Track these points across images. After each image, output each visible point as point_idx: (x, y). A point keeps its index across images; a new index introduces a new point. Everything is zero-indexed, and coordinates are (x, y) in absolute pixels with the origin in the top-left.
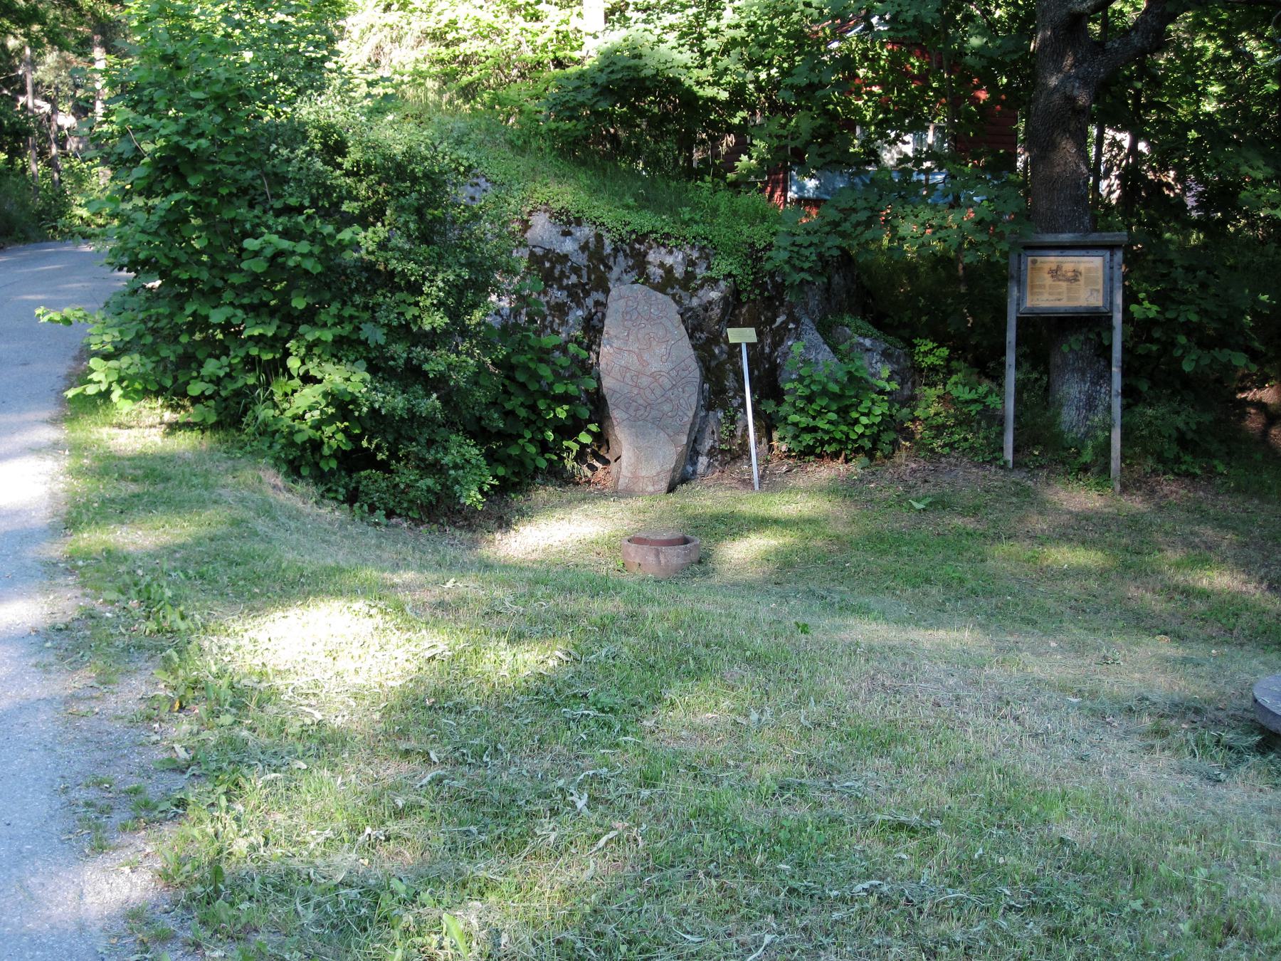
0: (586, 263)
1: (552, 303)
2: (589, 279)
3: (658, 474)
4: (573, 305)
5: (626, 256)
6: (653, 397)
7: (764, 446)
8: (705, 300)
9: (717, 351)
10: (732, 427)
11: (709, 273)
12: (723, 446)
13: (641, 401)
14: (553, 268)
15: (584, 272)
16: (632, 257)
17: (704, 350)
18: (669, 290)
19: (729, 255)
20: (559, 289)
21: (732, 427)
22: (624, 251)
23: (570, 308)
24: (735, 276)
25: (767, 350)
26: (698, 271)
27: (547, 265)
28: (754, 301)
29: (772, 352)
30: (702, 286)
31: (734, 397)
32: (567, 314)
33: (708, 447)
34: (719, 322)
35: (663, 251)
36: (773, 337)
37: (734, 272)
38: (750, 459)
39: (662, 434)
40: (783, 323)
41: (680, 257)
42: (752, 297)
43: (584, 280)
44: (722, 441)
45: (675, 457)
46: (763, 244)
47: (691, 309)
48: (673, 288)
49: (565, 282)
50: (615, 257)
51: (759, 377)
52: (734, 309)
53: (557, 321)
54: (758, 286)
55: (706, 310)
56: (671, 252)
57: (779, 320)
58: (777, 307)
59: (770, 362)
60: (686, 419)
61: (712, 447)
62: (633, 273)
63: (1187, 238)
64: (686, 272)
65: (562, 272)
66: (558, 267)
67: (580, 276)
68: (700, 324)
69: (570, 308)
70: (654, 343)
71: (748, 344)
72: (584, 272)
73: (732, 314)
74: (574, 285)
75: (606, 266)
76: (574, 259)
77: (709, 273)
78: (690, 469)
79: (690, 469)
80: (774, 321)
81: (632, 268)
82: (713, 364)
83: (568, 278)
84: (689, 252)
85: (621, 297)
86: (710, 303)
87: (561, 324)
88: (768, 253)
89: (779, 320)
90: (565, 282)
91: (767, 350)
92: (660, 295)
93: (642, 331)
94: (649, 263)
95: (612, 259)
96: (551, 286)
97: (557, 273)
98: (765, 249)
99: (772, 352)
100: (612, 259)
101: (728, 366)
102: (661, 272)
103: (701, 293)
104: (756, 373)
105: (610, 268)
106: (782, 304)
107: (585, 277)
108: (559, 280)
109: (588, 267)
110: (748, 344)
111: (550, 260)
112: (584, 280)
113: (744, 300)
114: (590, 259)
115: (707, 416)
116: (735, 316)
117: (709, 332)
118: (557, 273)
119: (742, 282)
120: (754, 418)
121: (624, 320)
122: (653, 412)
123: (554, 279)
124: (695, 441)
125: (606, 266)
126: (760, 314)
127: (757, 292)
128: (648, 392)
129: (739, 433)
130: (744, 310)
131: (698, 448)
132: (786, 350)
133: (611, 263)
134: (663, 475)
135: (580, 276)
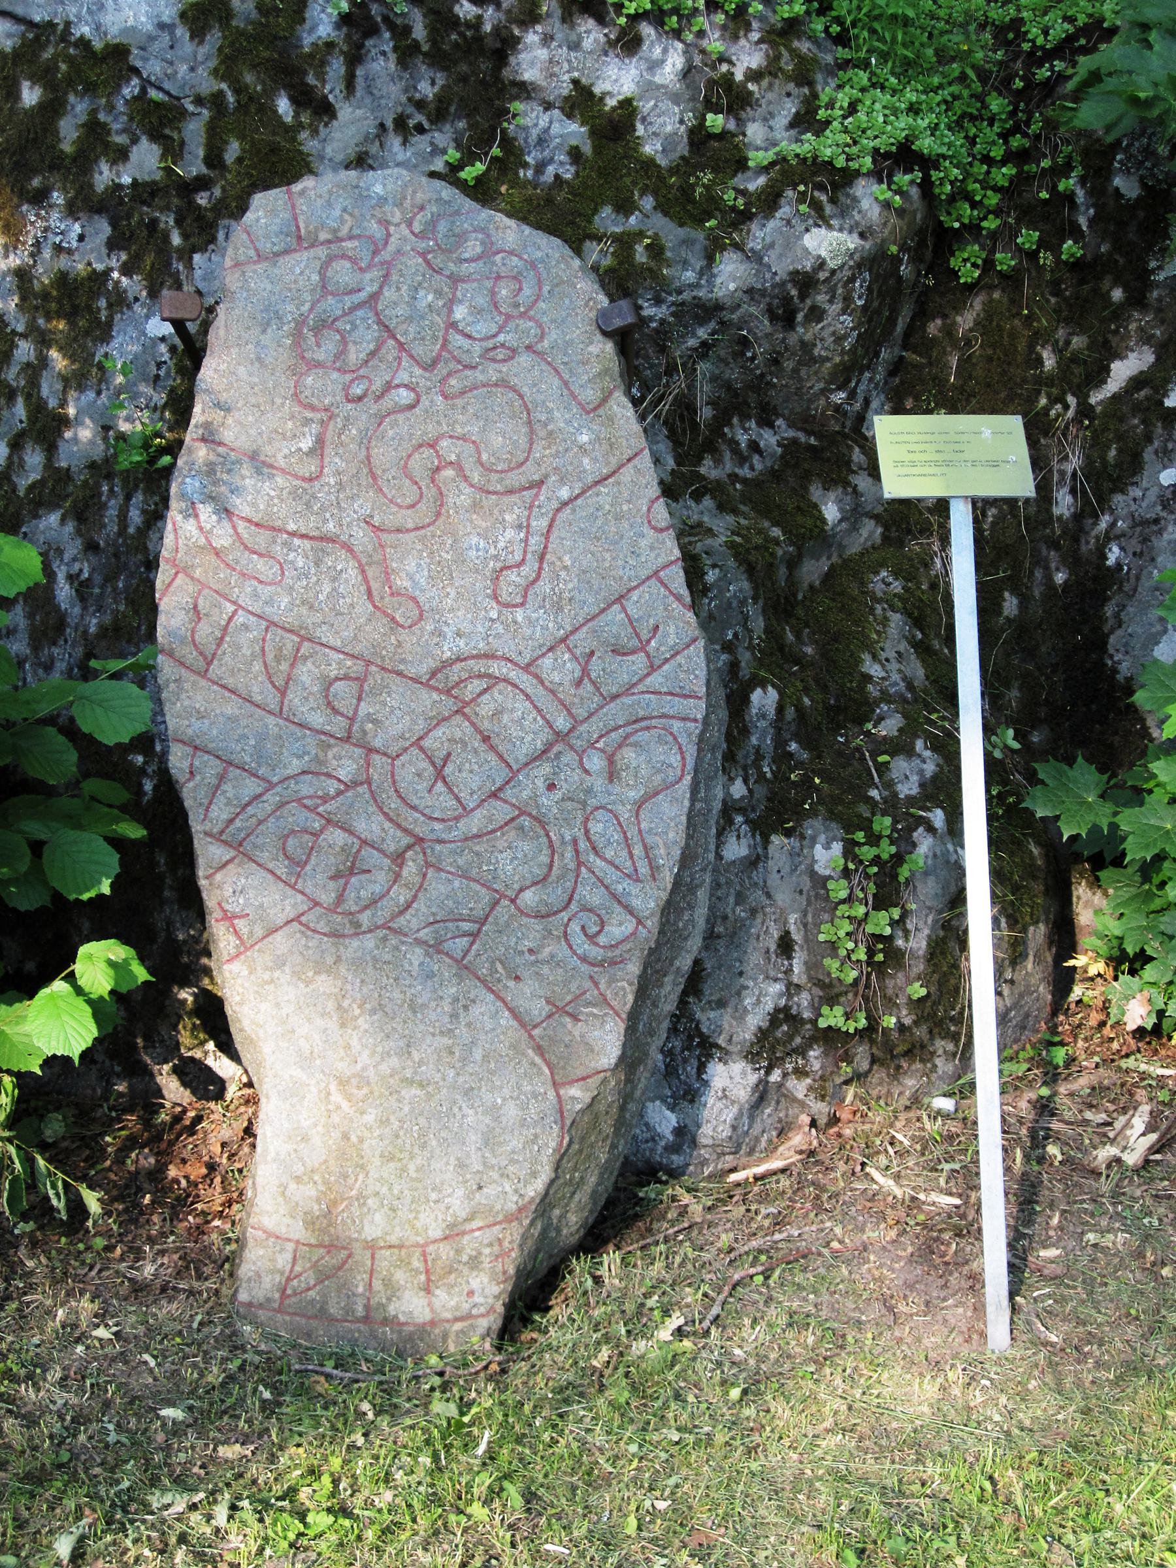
0: (207, 84)
1: (43, 276)
2: (214, 159)
3: (453, 1233)
4: (132, 285)
5: (406, 53)
6: (442, 802)
7: (1033, 971)
8: (781, 266)
9: (831, 512)
10: (881, 923)
11: (808, 144)
12: (833, 1017)
13: (370, 825)
14: (52, 108)
15: (194, 131)
16: (438, 58)
17: (765, 509)
18: (607, 219)
19: (908, 69)
20: (71, 211)
21: (881, 923)
22: (401, 32)
23: (120, 301)
24: (927, 163)
25: (1064, 504)
26: (755, 131)
27: (30, 96)
28: (1011, 280)
29: (1086, 513)
30: (769, 201)
31: (900, 746)
32: (104, 332)
33: (755, 1020)
34: (844, 376)
35: (591, 33)
36: (1096, 445)
37: (925, 144)
38: (965, 1055)
39: (484, 1008)
40: (1137, 382)
41: (675, 61)
42: (1005, 260)
43: (193, 166)
44: (830, 993)
45: (551, 1141)
46: (1060, 30)
47: (708, 311)
48: (625, 207)
49: (104, 175)
50: (355, 58)
51: (1022, 628)
52: (922, 314)
53: (58, 360)
54: (1030, 214)
55: (784, 315)
56: (629, 43)
57: (1122, 371)
58: (1118, 314)
59: (1073, 561)
60: (619, 928)
61: (782, 1015)
62: (442, 138)
63: (1058, 351)
64: (699, 137)
65: (94, 130)
66: (79, 107)
67: (173, 150)
68: (759, 385)
69: (120, 301)
70: (460, 497)
71: (980, 506)
72: (194, 131)
73: (913, 337)
74: (144, 192)
75: (305, 99)
76: (153, 68)
77: (808, 144)
78: (665, 1120)
79: (665, 1120)
80: (1100, 374)
81: (439, 113)
82: (813, 570)
83: (121, 155)
84: (715, 44)
85: (300, 240)
86: (805, 281)
87: (75, 381)
88: (1085, 63)
89: (1122, 371)
90: (104, 175)
91: (1064, 504)
92: (548, 247)
93: (400, 429)
94: (524, 90)
95: (337, 67)
96: (39, 198)
97: (69, 131)
98: (1067, 48)
99: (1086, 513)
100: (337, 67)
101: (886, 582)
102: (574, 131)
103: (760, 234)
104: (1010, 605)
105: (325, 111)
106: (1137, 300)
107: (197, 150)
108: (83, 161)
109: (217, 100)
110: (980, 506)
111: (44, 76)
112: (193, 166)
113: (969, 274)
114: (227, 68)
115: (754, 862)
116: (927, 346)
117: (803, 421)
118: (69, 131)
119: (961, 194)
120: (994, 843)
121: (304, 363)
122: (437, 886)
123: (57, 163)
124: (694, 982)
125: (305, 99)
126: (1038, 337)
127: (1028, 238)
128: (411, 771)
129: (917, 943)
130: (965, 321)
131: (706, 1018)
132: (1149, 508)
133: (332, 87)
134: (476, 1241)
135: (173, 150)
